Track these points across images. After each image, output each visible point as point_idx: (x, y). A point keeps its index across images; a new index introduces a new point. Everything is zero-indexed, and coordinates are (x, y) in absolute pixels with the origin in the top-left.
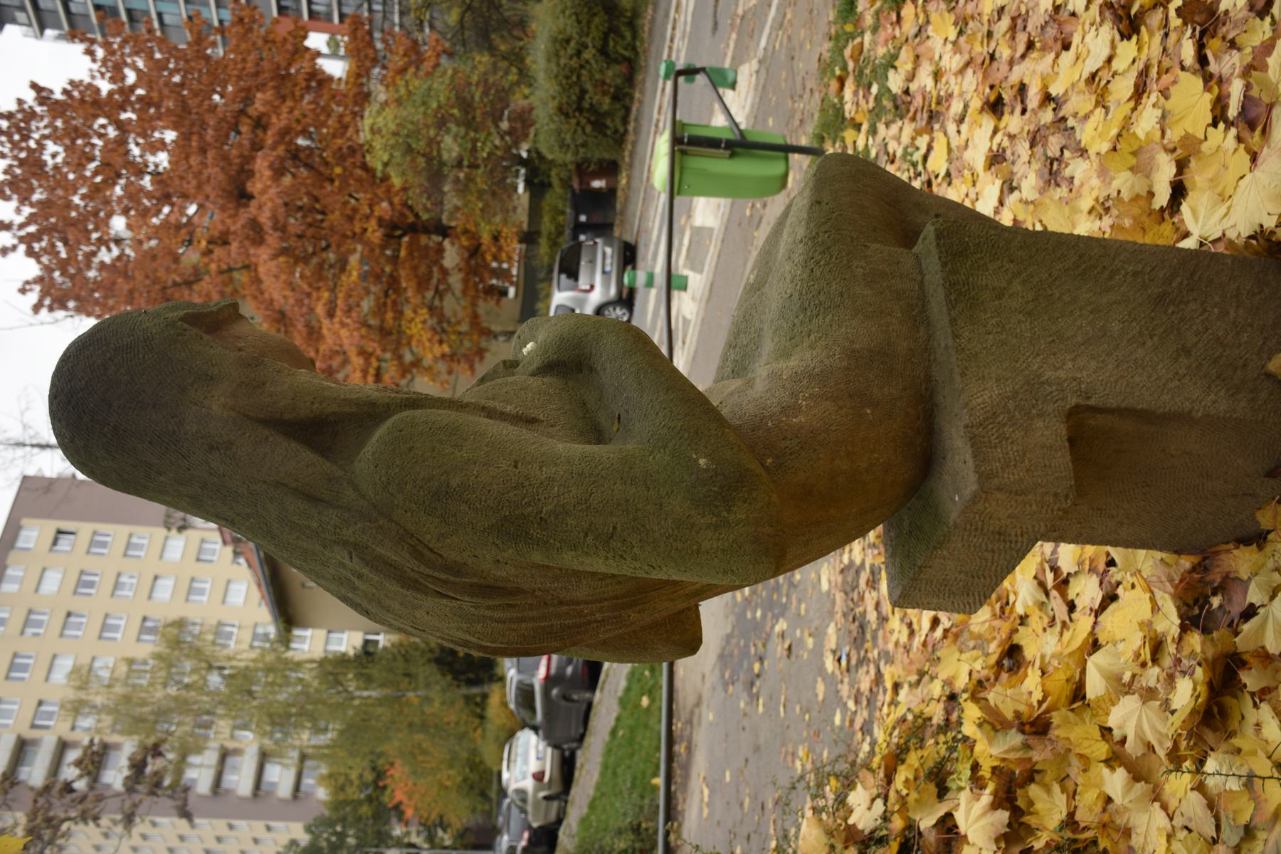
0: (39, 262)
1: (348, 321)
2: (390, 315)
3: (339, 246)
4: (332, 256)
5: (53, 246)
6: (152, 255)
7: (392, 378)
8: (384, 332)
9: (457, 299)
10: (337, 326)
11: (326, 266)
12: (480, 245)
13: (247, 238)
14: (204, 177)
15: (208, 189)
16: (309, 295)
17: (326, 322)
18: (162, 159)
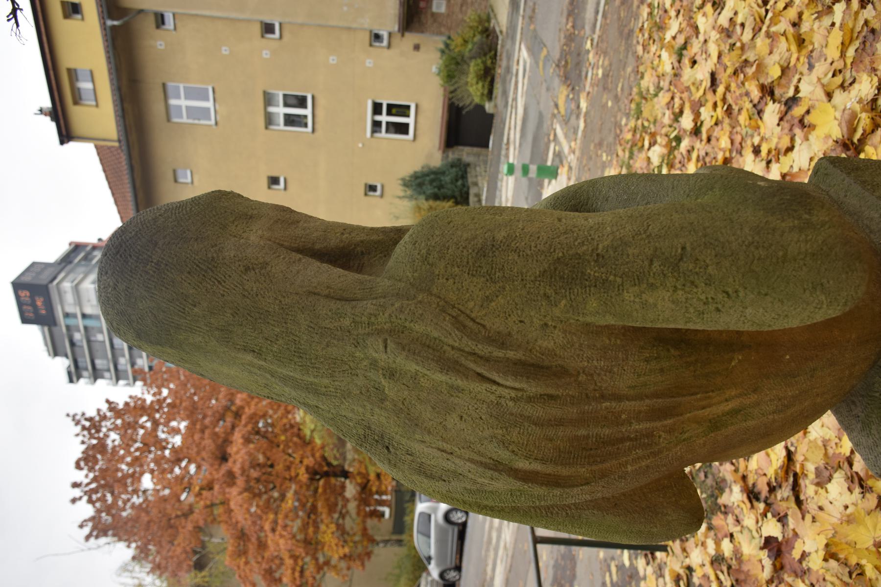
0: (94, 506)
1: (285, 533)
2: (311, 530)
3: (281, 485)
4: (276, 494)
5: (104, 496)
6: (164, 499)
7: (311, 572)
8: (307, 542)
9: (353, 520)
10: (278, 537)
11: (272, 500)
12: (368, 481)
13: (225, 482)
14: (202, 446)
15: (204, 454)
16: (261, 518)
17: (270, 535)
18: (177, 440)
